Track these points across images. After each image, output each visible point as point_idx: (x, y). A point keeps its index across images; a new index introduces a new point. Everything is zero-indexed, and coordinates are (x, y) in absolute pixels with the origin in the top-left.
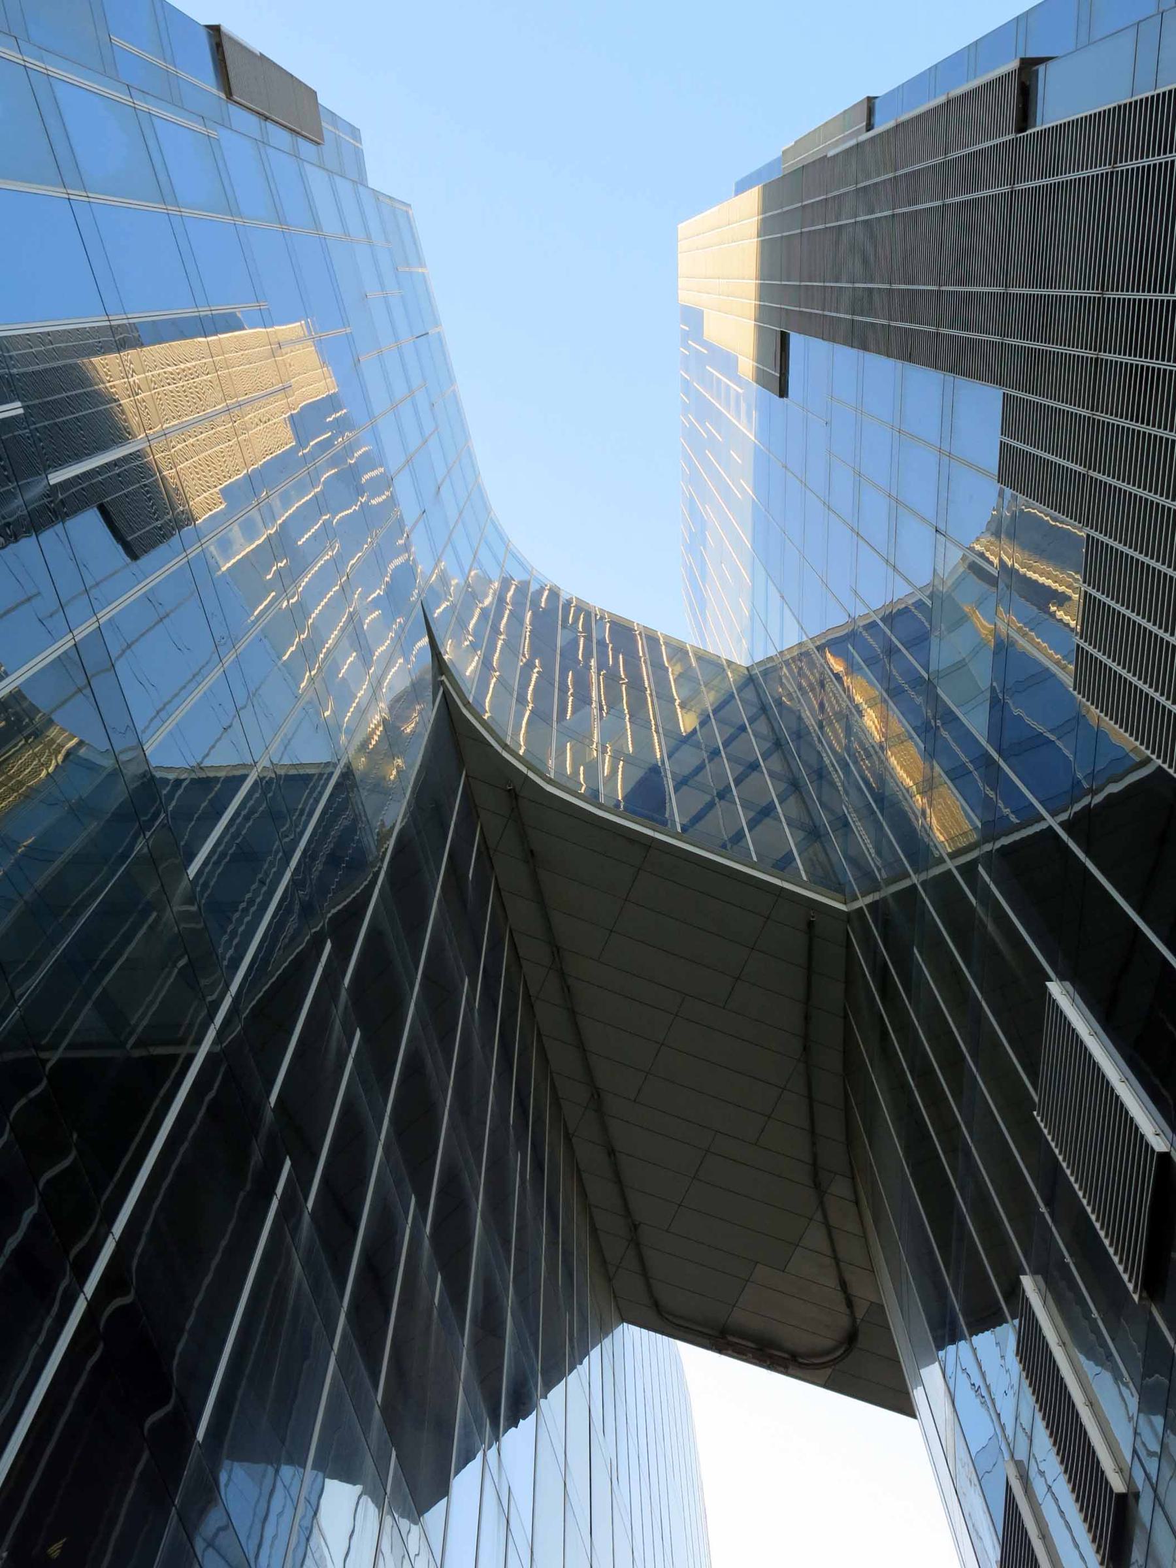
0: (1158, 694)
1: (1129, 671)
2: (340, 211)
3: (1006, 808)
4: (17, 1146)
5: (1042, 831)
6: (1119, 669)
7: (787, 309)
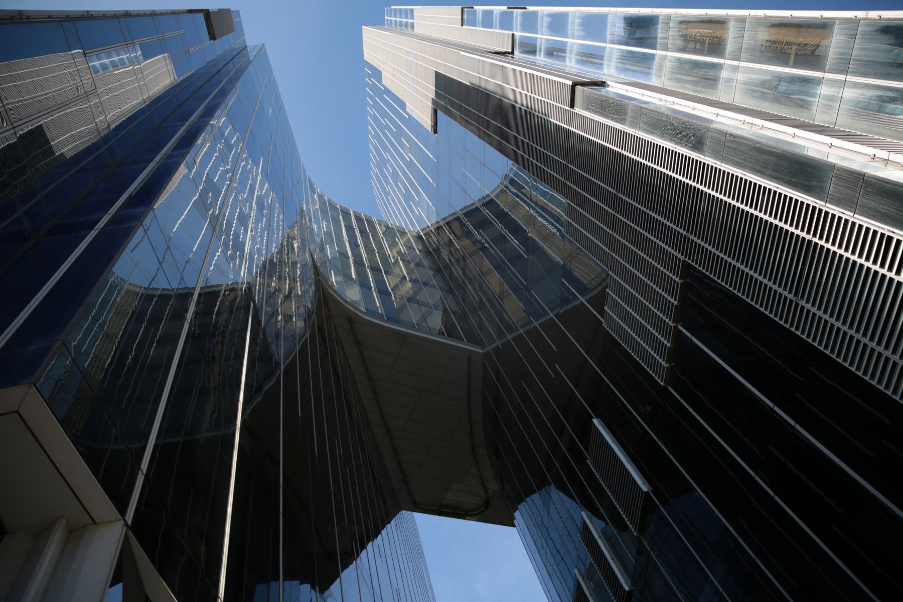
0: (620, 237)
1: (597, 220)
2: (34, 119)
3: (531, 236)
4: (211, 122)
5: (594, 295)
6: (587, 215)
7: (407, 51)
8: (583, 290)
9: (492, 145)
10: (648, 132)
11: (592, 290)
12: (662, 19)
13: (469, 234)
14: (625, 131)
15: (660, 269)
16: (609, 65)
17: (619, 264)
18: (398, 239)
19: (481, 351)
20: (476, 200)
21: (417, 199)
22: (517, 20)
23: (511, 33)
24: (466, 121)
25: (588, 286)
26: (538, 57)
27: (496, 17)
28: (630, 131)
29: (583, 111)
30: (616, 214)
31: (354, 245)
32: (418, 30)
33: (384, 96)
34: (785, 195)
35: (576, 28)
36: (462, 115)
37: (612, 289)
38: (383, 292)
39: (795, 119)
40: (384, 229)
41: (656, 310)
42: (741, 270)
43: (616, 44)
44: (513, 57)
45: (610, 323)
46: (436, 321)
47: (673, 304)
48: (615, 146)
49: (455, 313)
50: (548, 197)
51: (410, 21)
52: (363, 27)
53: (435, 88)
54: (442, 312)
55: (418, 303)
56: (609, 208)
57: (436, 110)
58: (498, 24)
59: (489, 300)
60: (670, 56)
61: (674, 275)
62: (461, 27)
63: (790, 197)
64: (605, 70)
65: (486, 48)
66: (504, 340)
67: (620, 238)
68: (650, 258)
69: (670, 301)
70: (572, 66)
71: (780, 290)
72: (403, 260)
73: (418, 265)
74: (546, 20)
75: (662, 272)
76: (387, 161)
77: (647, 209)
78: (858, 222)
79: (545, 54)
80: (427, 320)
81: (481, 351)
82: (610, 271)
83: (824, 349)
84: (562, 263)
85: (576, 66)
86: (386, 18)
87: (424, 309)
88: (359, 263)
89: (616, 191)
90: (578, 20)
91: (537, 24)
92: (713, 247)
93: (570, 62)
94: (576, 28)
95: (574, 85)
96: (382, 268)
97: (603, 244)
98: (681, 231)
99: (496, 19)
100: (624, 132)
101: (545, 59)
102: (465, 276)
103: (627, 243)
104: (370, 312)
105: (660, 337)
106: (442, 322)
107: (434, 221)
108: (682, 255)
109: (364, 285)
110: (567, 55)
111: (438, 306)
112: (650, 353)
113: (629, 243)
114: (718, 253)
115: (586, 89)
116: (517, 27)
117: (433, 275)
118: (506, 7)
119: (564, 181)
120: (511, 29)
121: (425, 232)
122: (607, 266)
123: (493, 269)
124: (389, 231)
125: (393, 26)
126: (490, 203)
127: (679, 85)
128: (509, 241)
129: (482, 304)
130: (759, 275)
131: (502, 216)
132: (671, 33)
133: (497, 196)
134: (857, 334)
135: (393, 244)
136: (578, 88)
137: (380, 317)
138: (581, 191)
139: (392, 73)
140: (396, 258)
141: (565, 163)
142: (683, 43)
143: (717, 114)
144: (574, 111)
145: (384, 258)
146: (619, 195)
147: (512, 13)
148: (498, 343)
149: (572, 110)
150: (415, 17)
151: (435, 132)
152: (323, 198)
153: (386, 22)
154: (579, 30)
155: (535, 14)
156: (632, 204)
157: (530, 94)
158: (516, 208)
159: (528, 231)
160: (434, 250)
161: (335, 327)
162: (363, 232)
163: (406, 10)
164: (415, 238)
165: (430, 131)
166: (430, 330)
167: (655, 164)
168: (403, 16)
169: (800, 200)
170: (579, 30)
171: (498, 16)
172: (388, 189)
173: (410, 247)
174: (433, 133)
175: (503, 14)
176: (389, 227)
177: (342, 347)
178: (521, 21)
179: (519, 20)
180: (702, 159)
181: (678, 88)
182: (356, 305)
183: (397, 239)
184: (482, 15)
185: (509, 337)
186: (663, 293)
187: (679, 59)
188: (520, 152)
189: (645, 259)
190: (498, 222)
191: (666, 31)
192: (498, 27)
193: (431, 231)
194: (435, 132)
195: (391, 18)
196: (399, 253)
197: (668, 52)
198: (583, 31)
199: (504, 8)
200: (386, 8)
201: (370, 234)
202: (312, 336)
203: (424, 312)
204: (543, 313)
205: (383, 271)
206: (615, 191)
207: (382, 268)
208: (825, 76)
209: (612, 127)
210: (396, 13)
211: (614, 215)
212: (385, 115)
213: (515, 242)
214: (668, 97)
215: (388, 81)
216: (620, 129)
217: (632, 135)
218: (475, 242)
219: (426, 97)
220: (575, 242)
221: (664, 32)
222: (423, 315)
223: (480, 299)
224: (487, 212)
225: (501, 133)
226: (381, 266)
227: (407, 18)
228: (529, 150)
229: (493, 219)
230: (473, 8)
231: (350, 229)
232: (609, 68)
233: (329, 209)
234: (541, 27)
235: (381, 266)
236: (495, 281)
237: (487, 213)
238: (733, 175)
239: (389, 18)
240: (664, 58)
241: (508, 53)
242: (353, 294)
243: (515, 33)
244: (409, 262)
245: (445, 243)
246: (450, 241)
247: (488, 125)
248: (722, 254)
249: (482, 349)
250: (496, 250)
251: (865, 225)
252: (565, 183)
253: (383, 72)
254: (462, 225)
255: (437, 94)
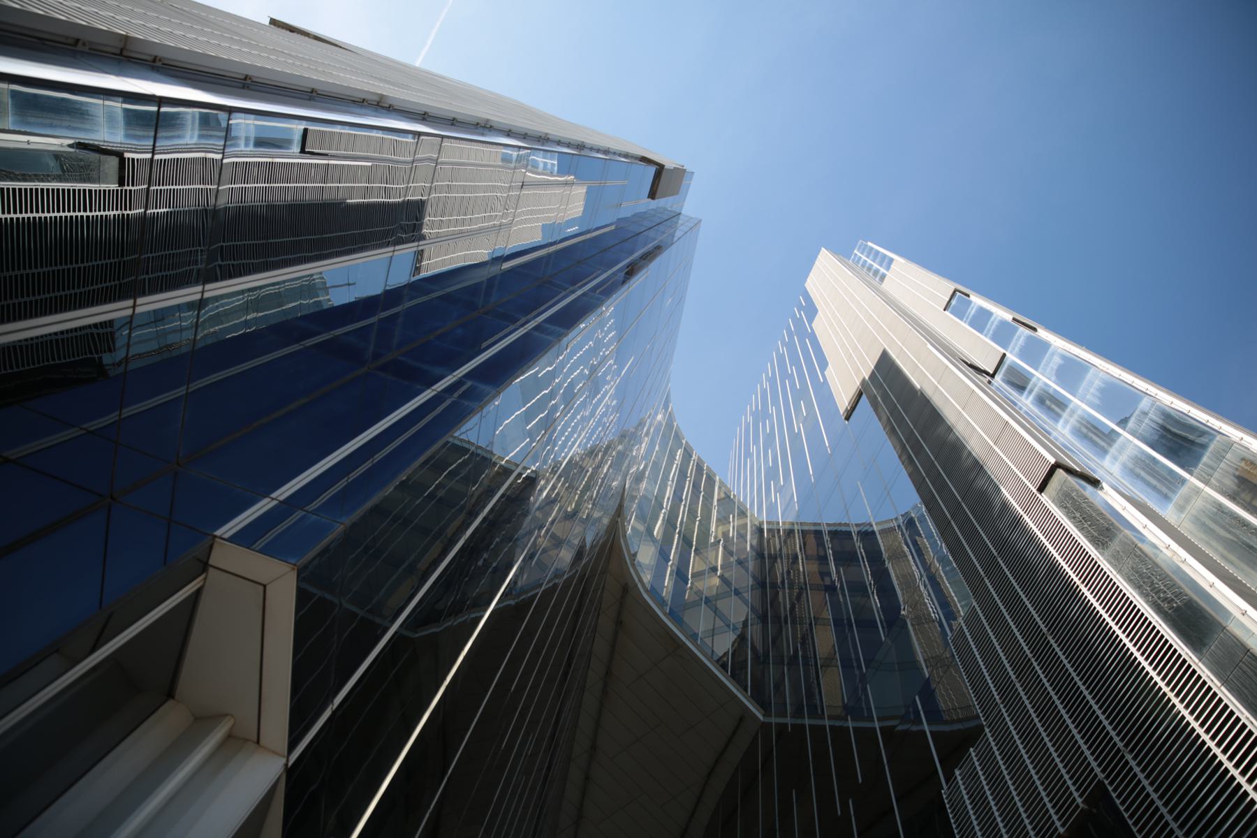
8: (934, 714)
9: (910, 475)
10: (1130, 580)
11: (946, 722)
12: (1218, 441)
13: (823, 559)
14: (1099, 563)
15: (1030, 715)
16: (1115, 459)
17: (989, 695)
18: (734, 517)
19: (761, 718)
20: (854, 522)
21: (782, 484)
22: (1018, 340)
23: (1003, 351)
24: (910, 457)
25: (943, 714)
26: (1023, 398)
27: (993, 323)
28: (1106, 566)
29: (1052, 505)
30: (1033, 660)
31: (677, 497)
32: (886, 286)
33: (807, 340)
34: (1215, 692)
35: (1092, 390)
36: (891, 419)
37: (979, 752)
38: (681, 575)
39: (1250, 588)
40: (723, 495)
41: (995, 748)
42: (1137, 779)
43: (1137, 438)
44: (990, 382)
45: (953, 796)
46: (724, 644)
47: (1056, 829)
48: (1077, 576)
49: (754, 648)
50: (948, 568)
51: (882, 270)
52: (823, 248)
53: (875, 367)
54: (736, 637)
55: (716, 610)
56: (1016, 627)
57: (862, 394)
58: (991, 332)
59: (805, 657)
60: (1207, 493)
61: (1050, 741)
62: (942, 310)
63: (1204, 681)
64: (1107, 462)
65: (961, 353)
66: (799, 721)
67: (1002, 655)
68: (1053, 746)
69: (1017, 746)
70: (1063, 432)
71: (1164, 810)
72: (725, 547)
73: (740, 562)
74: (1057, 360)
75: (1059, 770)
76: (770, 416)
77: (1056, 642)
78: (1220, 695)
79: (1035, 399)
80: (715, 637)
81: (761, 718)
82: (988, 727)
83: (1133, 824)
84: (927, 676)
85: (1069, 436)
86: (856, 251)
87: (719, 623)
88: (670, 523)
89: (1049, 630)
90: (1101, 384)
91: (1043, 359)
92: (1104, 713)
93: (1064, 427)
94: (1092, 390)
95: (1057, 466)
96: (694, 543)
97: (984, 665)
98: (1043, 626)
99: (992, 326)
100: (1096, 562)
101: (1031, 406)
102: (791, 614)
103: (981, 615)
104: (654, 592)
105: (990, 798)
106: (733, 646)
107: (790, 520)
108: (1103, 771)
109: (663, 555)
110: (1065, 415)
111: (737, 629)
112: (963, 796)
113: (997, 641)
114: (1071, 670)
115: (1070, 478)
116: (1014, 349)
117: (752, 586)
118: (1011, 317)
119: (983, 575)
120: (1004, 347)
121: (771, 527)
122: (987, 718)
123: (831, 621)
124: (727, 500)
125: (859, 265)
126: (868, 535)
127: (1204, 537)
128: (860, 566)
129: (793, 660)
130: (1116, 735)
131: (875, 558)
132: (1222, 465)
133: (882, 532)
134: (1158, 801)
135: (723, 520)
136: (1060, 472)
137: (662, 603)
138: (961, 538)
139: (830, 320)
140: (718, 539)
141: (1045, 630)
142: (1236, 488)
143: (1244, 612)
144: (1040, 497)
145: (705, 532)
146: (999, 559)
147: (1016, 329)
148: (788, 720)
149: (1038, 495)
150: (891, 269)
151: (847, 418)
152: (672, 423)
153: (853, 257)
154: (1093, 395)
155: (1045, 346)
156: (1037, 623)
157: (992, 444)
158: (901, 560)
159: (902, 608)
160: (770, 555)
161: (612, 548)
162: (696, 486)
163: (884, 256)
164: (754, 528)
165: (842, 413)
166: (712, 654)
167: (1124, 632)
168: (878, 260)
169: (1231, 707)
170: (1093, 395)
171: (996, 323)
172: (753, 449)
173: (742, 536)
174: (843, 418)
175: (1003, 323)
176: (729, 497)
177: (598, 615)
178: (1023, 345)
179: (1021, 341)
180: (1195, 662)
181: (1201, 540)
182: (638, 568)
183: (731, 516)
184: (976, 311)
185: (807, 722)
186: (1049, 806)
187: (1220, 507)
188: (942, 506)
189: (1023, 702)
190: (869, 572)
191: (1218, 459)
192: (989, 335)
193: (779, 531)
194: (847, 418)
195: (861, 255)
196: (725, 535)
197: (1207, 487)
198: (1100, 399)
199: (1008, 316)
200: (861, 241)
201: (702, 494)
202: (568, 583)
203: (716, 626)
204: (866, 715)
205: (694, 548)
206: (1046, 629)
207: (694, 543)
208: (1205, 489)
209: (1087, 553)
210: (864, 249)
211: (1029, 660)
212: (795, 361)
213: (876, 601)
214: (1180, 548)
215: (821, 326)
216: (1093, 556)
217: (1105, 573)
218: (825, 574)
219: (857, 371)
220: (952, 647)
221: (1215, 459)
222: (714, 629)
223: (796, 651)
224: (859, 545)
225: (930, 468)
226: (695, 540)
227: (881, 266)
228: (956, 510)
229: (863, 558)
230: (968, 296)
231: (682, 474)
232: (1113, 464)
233: (671, 435)
234: (1047, 365)
235: (695, 540)
236: (825, 640)
237: (861, 553)
238: (1175, 651)
239: (859, 254)
240: (1198, 491)
241: (987, 373)
242: (646, 555)
243: (1008, 355)
244: (731, 554)
245: (788, 554)
246: (796, 557)
247: (918, 449)
248: (1087, 692)
249: (764, 716)
250: (846, 600)
251: (1225, 701)
252: (983, 579)
253: (819, 311)
254: (820, 543)
255: (873, 376)
